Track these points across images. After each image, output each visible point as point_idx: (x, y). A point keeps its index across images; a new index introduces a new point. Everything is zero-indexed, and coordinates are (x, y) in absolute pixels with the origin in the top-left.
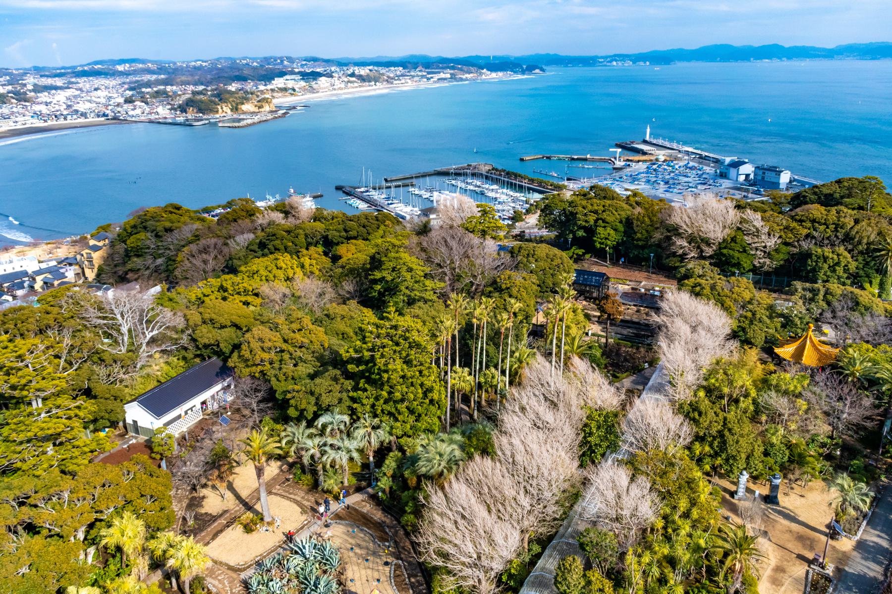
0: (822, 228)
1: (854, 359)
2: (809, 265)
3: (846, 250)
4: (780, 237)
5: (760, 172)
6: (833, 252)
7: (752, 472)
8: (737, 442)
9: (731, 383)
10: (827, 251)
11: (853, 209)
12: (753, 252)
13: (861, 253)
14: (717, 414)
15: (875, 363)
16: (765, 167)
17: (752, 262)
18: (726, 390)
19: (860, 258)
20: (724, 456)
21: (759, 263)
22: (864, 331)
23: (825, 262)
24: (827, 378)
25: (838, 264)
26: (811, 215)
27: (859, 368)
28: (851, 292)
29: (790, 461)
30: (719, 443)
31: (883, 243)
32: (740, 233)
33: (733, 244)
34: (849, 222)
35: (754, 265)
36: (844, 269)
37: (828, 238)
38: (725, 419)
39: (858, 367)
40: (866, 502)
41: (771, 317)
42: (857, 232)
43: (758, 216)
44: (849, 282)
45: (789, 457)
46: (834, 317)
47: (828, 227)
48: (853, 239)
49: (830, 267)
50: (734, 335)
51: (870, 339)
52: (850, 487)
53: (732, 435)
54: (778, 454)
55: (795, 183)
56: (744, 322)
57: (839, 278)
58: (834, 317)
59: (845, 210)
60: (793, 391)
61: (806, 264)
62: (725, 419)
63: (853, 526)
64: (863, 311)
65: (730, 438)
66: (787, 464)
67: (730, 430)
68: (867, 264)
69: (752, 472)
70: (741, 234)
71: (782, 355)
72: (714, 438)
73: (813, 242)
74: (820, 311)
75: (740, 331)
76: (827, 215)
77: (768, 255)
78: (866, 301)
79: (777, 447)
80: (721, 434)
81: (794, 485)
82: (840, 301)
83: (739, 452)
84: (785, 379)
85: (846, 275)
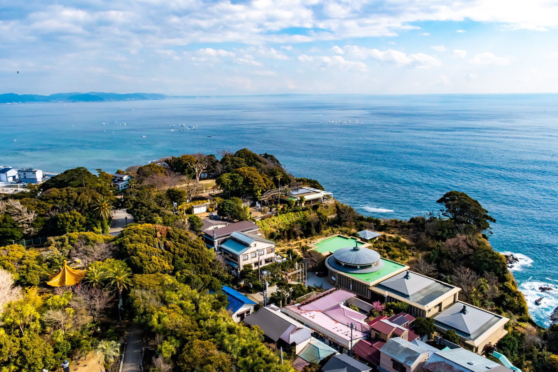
0: (60, 201)
1: (93, 272)
2: (59, 225)
3: (77, 211)
4: (36, 212)
5: (22, 174)
6: (71, 214)
7: (50, 367)
8: (33, 353)
9: (22, 316)
10: (67, 214)
11: (76, 187)
12: (21, 226)
13: (86, 211)
14: (14, 341)
15: (105, 270)
16: (24, 170)
17: (22, 232)
18: (19, 322)
19: (87, 214)
20: (26, 367)
21: (27, 231)
22: (96, 255)
23: (67, 221)
24: (81, 289)
25: (75, 220)
26: (51, 195)
27: (97, 277)
28: (83, 235)
29: (73, 348)
30: (20, 359)
31: (96, 203)
32: (8, 216)
33: (5, 224)
34: (75, 195)
35: (24, 234)
36: (80, 222)
37: (66, 207)
38: (21, 341)
39: (96, 276)
40: (117, 351)
41: (40, 264)
42: (81, 200)
43: (18, 202)
44: (84, 229)
45: (71, 346)
46: (78, 252)
47: (63, 200)
48: (79, 204)
49: (71, 223)
50: (17, 283)
51: (100, 258)
52: (106, 347)
53: (29, 350)
54: (63, 347)
55: (46, 177)
56: (22, 273)
57: (78, 228)
58: (78, 252)
59: (71, 189)
60: (63, 304)
61: (57, 225)
62: (21, 341)
63: (116, 368)
64: (92, 243)
65: (27, 353)
66: (71, 351)
67: (26, 348)
68: (91, 216)
69: (50, 367)
70: (9, 216)
71: (53, 285)
72: (16, 358)
73: (58, 211)
74: (68, 251)
75: (21, 279)
76: (61, 193)
77: (32, 225)
78: (92, 237)
79: (62, 344)
80: (20, 353)
81: (79, 362)
82: (79, 241)
83: (36, 359)
84: (57, 299)
85: (81, 226)
